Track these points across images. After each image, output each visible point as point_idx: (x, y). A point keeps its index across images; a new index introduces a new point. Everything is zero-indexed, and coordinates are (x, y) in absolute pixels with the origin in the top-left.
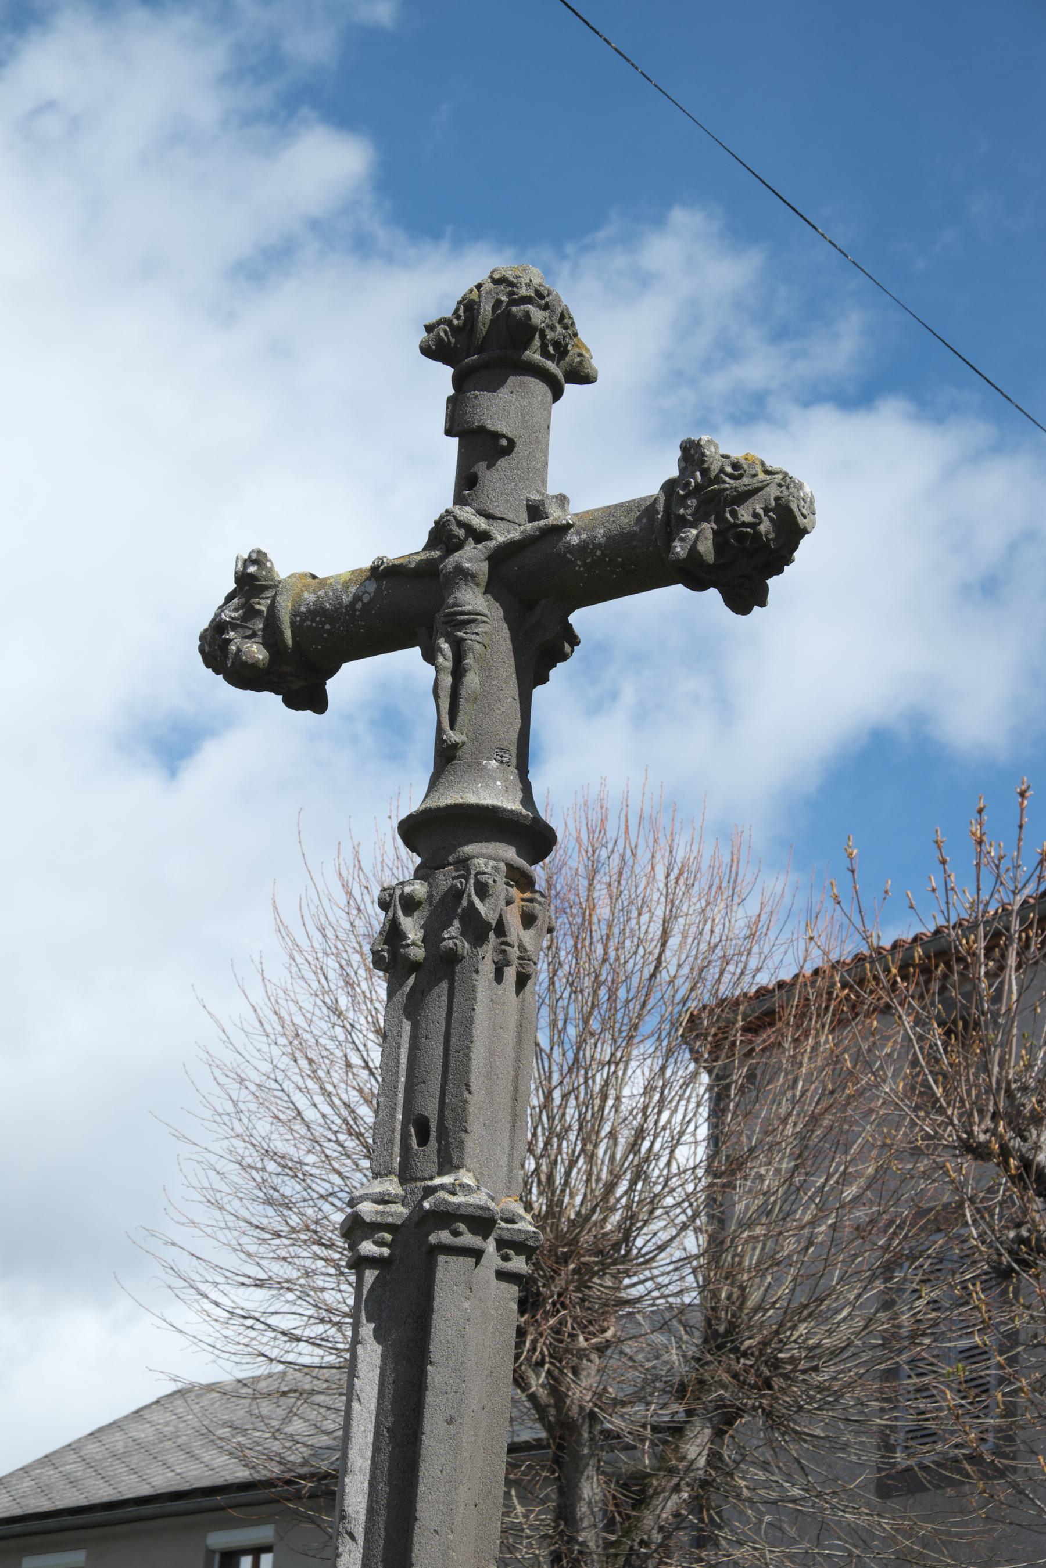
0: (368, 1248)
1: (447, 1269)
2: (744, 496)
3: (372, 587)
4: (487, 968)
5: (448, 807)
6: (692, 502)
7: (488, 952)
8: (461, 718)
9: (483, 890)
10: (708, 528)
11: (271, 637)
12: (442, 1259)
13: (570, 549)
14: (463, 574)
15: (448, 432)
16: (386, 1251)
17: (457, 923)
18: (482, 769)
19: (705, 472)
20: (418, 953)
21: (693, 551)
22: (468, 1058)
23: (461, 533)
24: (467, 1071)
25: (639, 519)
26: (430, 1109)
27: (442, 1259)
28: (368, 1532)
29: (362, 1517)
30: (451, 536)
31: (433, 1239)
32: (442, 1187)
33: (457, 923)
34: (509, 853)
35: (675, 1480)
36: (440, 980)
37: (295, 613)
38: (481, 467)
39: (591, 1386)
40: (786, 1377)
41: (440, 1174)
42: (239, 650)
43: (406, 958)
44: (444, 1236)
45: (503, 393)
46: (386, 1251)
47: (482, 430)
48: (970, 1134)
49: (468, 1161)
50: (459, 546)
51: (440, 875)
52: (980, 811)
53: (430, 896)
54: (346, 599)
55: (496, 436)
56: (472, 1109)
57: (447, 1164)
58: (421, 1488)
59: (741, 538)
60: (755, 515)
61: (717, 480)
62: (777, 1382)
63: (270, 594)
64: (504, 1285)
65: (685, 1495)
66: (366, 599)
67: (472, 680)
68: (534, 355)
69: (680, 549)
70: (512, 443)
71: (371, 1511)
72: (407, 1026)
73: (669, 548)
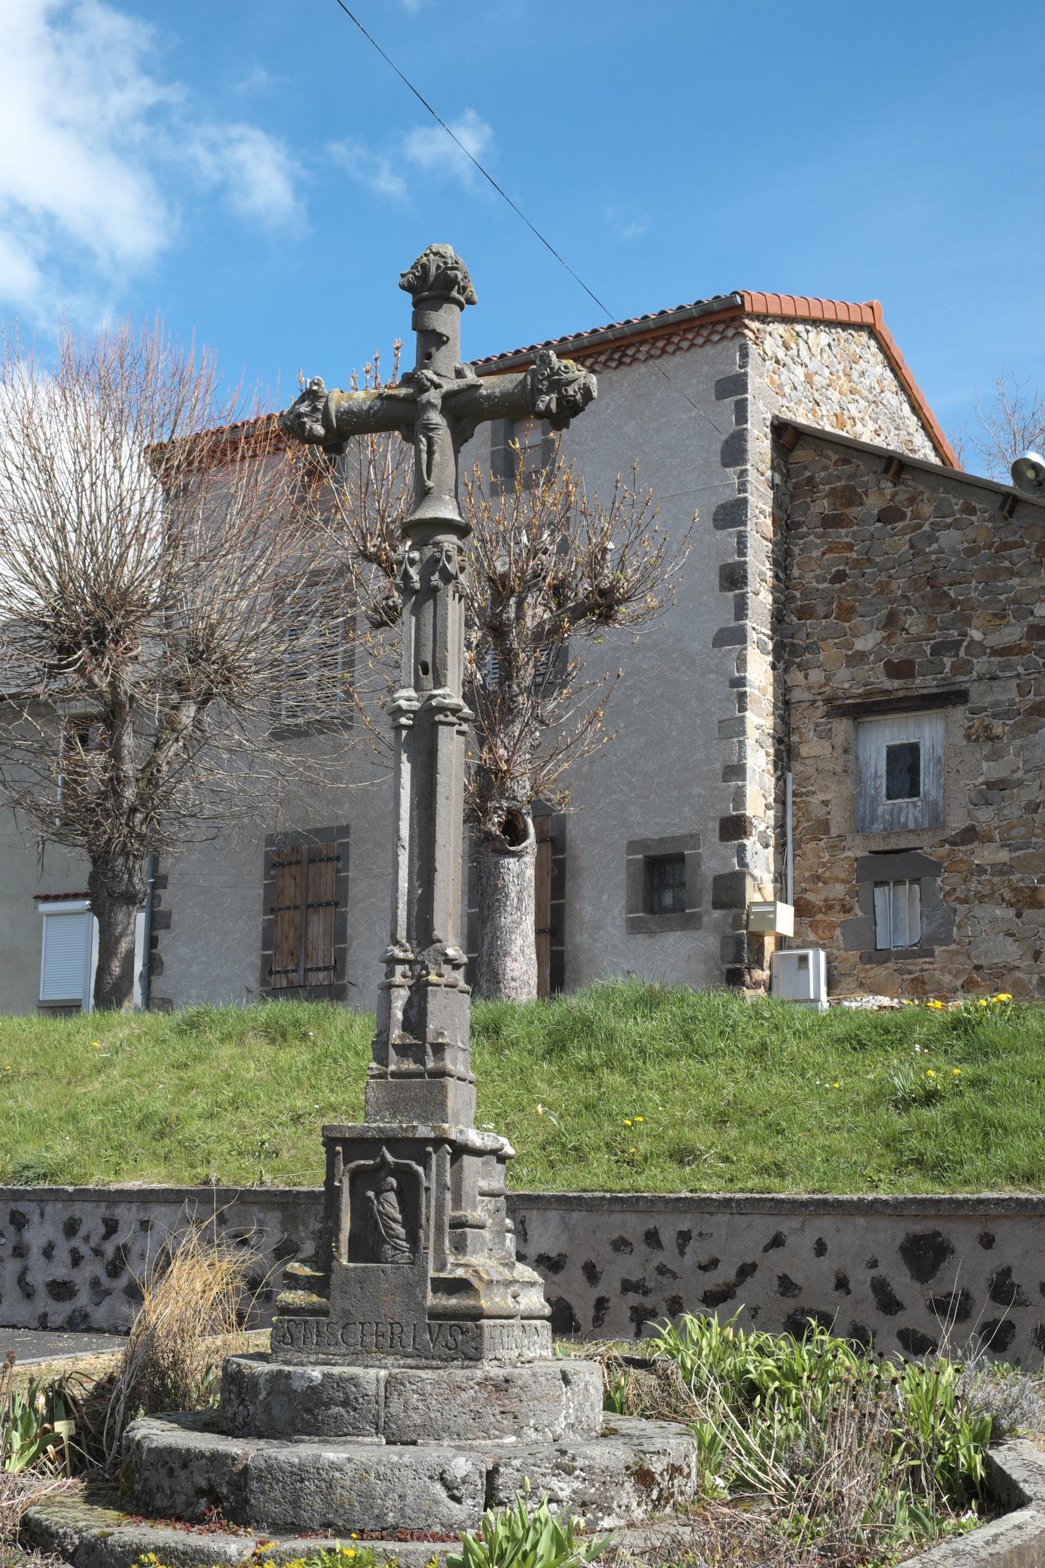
0: (403, 721)
1: (443, 731)
2: (570, 382)
3: (378, 403)
4: (451, 593)
5: (431, 519)
6: (545, 383)
7: (451, 587)
8: (433, 475)
9: (449, 559)
10: (554, 396)
11: (326, 422)
12: (440, 727)
13: (482, 396)
14: (430, 405)
15: (414, 329)
16: (411, 722)
17: (437, 573)
18: (443, 500)
19: (552, 369)
20: (417, 586)
21: (548, 406)
22: (446, 635)
23: (429, 384)
24: (446, 642)
25: (516, 387)
26: (429, 659)
27: (440, 727)
28: (410, 845)
29: (407, 839)
30: (424, 385)
31: (436, 718)
32: (439, 695)
33: (437, 573)
34: (454, 538)
35: (176, 735)
36: (428, 600)
37: (338, 411)
38: (433, 350)
39: (812, 867)
40: (239, 676)
41: (435, 688)
42: (311, 428)
43: (413, 588)
44: (440, 717)
45: (441, 312)
46: (411, 722)
47: (434, 331)
48: (365, 547)
49: (449, 683)
50: (427, 390)
51: (426, 549)
52: (376, 359)
53: (421, 559)
54: (365, 408)
55: (441, 335)
56: (449, 659)
57: (438, 683)
58: (437, 828)
59: (568, 402)
60: (575, 391)
61: (558, 374)
62: (234, 679)
63: (324, 400)
64: (459, 737)
65: (181, 744)
66: (375, 408)
67: (437, 457)
68: (455, 294)
69: (541, 406)
70: (448, 339)
71: (411, 837)
72: (414, 619)
73: (534, 404)
